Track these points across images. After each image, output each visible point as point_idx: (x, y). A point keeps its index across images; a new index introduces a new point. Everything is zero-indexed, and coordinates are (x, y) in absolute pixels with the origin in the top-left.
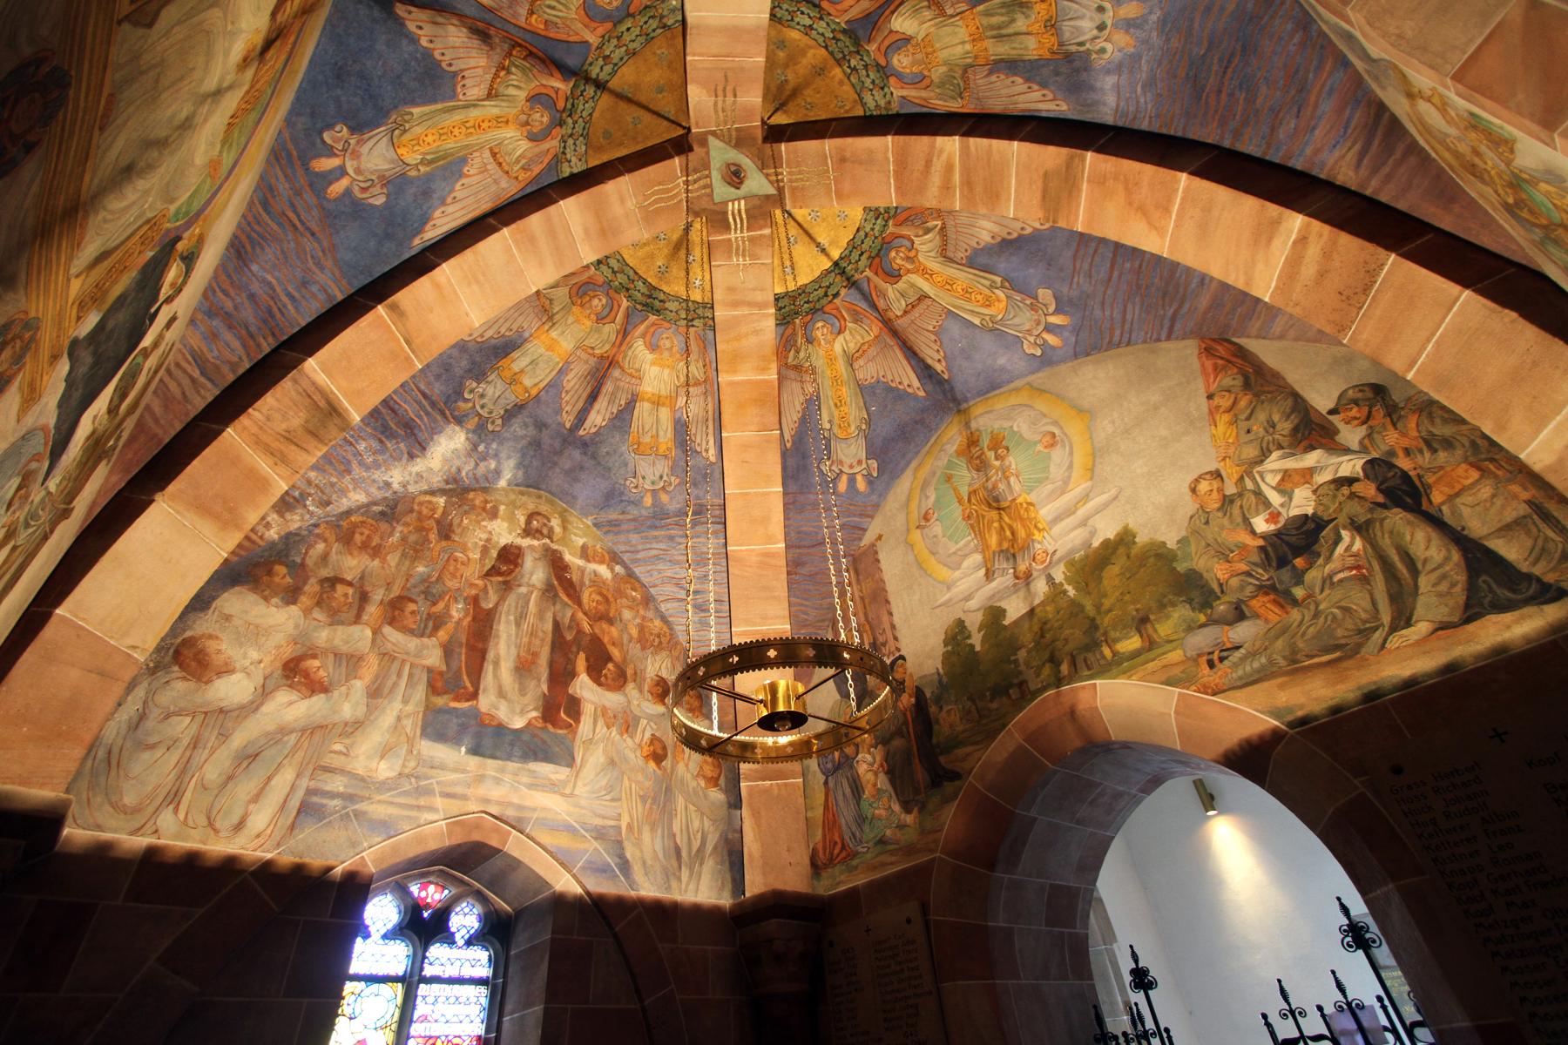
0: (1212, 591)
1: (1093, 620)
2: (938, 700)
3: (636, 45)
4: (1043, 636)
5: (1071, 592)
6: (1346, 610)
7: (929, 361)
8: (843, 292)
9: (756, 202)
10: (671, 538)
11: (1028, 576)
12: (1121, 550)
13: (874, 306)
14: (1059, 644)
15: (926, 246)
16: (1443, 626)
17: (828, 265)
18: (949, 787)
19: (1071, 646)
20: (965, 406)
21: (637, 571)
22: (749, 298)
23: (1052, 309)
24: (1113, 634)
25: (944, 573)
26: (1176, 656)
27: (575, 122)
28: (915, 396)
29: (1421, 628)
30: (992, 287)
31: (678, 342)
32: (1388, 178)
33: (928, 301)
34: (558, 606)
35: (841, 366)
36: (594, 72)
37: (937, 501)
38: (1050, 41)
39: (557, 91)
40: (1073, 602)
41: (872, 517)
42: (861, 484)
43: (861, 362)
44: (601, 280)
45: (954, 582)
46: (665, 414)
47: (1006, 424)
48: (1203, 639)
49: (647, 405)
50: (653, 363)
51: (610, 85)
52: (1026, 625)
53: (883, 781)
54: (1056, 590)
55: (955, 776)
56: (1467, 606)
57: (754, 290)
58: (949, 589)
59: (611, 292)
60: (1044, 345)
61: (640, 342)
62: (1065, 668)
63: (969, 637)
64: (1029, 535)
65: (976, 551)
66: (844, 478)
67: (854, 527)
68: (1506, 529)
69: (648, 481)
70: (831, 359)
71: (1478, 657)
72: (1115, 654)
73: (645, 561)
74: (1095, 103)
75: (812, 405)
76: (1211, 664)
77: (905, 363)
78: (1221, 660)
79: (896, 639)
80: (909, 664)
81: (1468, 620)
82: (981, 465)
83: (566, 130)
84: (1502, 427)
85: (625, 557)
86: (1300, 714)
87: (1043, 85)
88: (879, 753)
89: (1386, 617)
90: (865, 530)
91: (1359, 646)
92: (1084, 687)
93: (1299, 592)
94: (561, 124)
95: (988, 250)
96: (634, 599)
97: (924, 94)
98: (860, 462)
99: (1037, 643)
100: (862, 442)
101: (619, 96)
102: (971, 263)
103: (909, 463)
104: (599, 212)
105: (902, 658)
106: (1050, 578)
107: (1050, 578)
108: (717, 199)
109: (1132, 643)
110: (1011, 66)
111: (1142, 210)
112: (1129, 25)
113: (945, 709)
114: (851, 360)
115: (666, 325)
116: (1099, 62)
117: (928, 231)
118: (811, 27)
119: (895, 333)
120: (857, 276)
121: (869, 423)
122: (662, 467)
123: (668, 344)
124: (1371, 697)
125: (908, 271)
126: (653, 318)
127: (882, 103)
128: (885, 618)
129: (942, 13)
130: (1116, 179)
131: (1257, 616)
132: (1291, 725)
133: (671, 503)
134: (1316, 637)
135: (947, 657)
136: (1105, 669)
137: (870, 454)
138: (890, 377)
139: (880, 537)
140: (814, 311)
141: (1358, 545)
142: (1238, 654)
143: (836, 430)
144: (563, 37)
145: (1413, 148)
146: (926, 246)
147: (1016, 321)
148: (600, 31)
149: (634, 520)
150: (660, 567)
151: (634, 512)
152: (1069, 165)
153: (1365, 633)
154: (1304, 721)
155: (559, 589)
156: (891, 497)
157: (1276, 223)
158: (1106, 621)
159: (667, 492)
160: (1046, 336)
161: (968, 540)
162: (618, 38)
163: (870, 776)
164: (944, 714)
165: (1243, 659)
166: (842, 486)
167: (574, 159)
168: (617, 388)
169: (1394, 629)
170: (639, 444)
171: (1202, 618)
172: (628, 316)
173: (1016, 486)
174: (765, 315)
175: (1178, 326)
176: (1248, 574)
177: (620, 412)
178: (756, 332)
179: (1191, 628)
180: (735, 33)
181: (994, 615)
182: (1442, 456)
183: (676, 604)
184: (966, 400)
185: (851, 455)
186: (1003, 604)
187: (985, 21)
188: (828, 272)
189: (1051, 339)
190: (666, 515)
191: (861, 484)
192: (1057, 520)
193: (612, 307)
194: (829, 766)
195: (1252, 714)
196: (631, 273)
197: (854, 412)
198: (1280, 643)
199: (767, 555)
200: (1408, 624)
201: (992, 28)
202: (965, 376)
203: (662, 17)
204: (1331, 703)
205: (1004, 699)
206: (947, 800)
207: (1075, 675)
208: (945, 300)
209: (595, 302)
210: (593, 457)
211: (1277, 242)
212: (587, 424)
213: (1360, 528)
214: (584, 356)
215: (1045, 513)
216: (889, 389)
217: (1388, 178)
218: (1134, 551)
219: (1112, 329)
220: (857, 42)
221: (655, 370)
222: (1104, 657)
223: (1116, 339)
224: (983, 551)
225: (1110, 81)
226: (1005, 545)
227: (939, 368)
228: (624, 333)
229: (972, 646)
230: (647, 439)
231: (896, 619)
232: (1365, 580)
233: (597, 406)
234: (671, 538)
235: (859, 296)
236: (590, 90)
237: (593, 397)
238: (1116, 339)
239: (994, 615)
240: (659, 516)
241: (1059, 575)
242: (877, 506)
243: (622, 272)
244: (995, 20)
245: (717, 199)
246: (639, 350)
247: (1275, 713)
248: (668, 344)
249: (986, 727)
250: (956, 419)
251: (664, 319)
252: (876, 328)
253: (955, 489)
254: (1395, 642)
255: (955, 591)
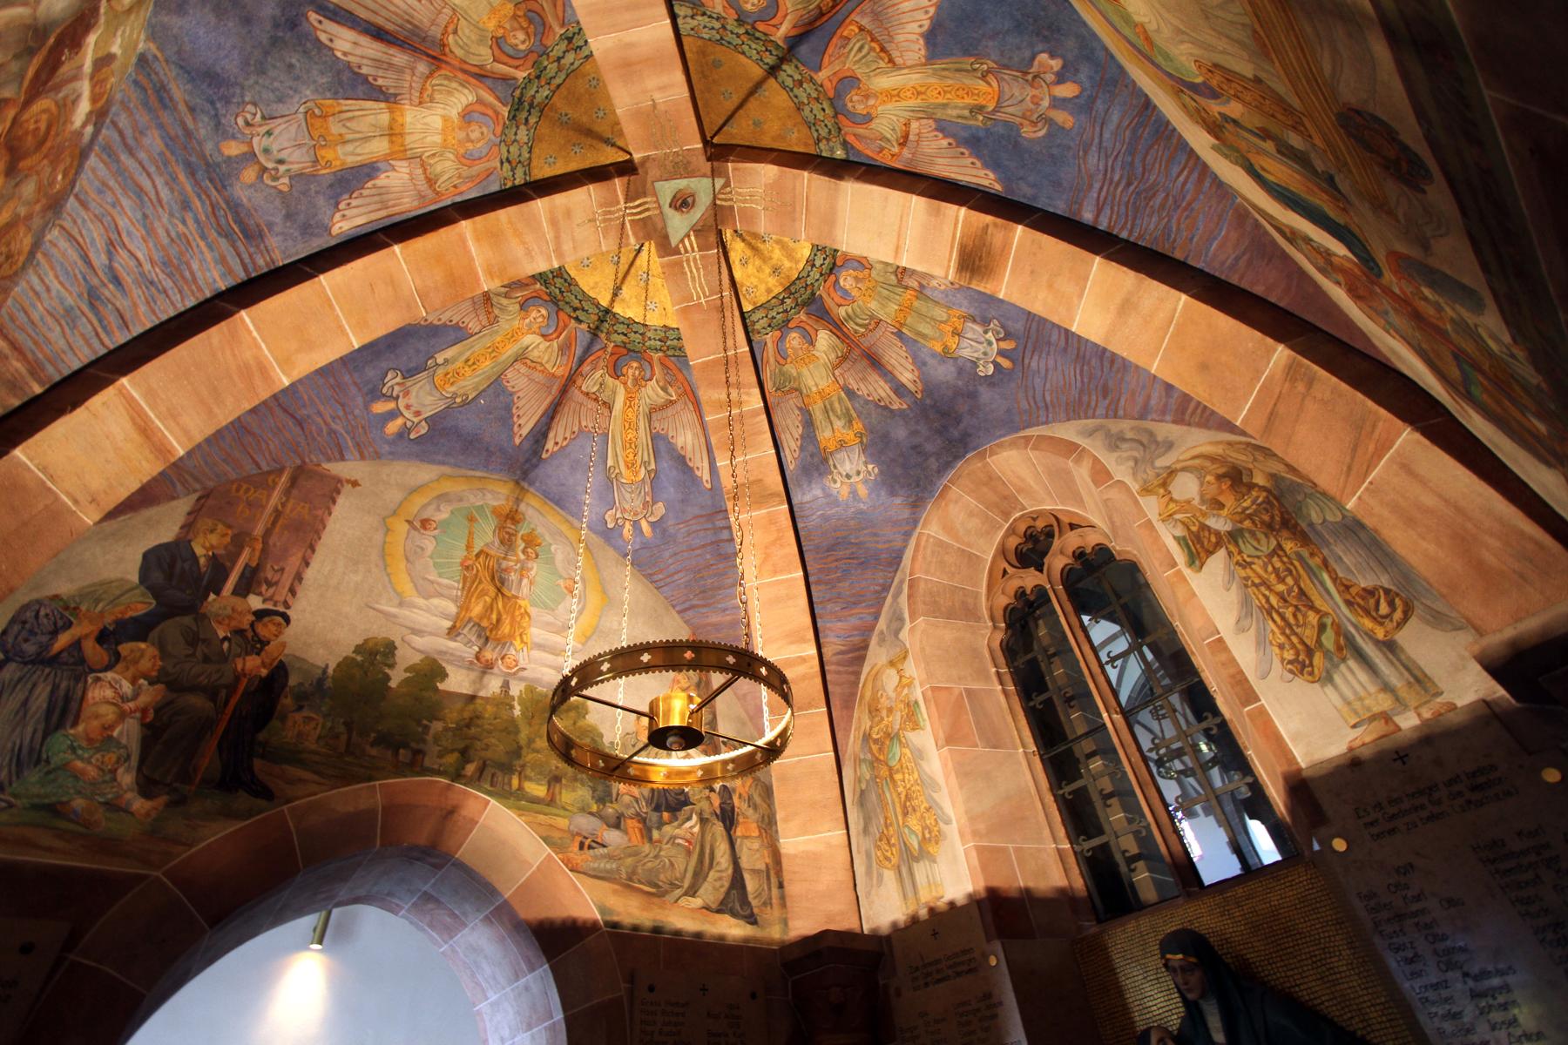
0: (610, 795)
1: (520, 748)
2: (302, 698)
3: (807, 111)
4: (468, 726)
5: (517, 712)
6: (672, 864)
7: (551, 435)
8: (584, 326)
9: (659, 226)
10: (186, 205)
11: (488, 667)
12: (572, 714)
13: (581, 362)
14: (478, 745)
15: (653, 392)
16: (707, 908)
17: (604, 303)
18: (243, 800)
19: (488, 754)
20: (526, 485)
21: (93, 161)
22: (563, 236)
23: (652, 519)
24: (528, 772)
25: (407, 587)
26: (562, 823)
27: (738, 36)
28: (512, 436)
29: (697, 902)
30: (645, 464)
31: (480, 147)
32: (838, 673)
33: (606, 412)
34: (14, 67)
35: (510, 351)
36: (788, 68)
37: (446, 523)
38: (832, 447)
39: (776, 27)
40: (513, 720)
41: (363, 458)
42: (393, 427)
43: (523, 369)
44: (548, 42)
45: (412, 606)
46: (379, 147)
47: (547, 537)
48: (586, 823)
49: (385, 118)
50: (445, 119)
51: (772, 81)
52: (459, 705)
53: (129, 732)
54: (504, 700)
55: (267, 794)
56: (721, 903)
57: (573, 240)
58: (401, 605)
59: (533, 57)
60: (619, 528)
61: (471, 98)
62: (470, 769)
63: (392, 666)
64: (511, 636)
65: (455, 600)
66: (391, 405)
67: (338, 445)
68: (755, 872)
69: (266, 142)
70: (513, 336)
71: (713, 937)
72: (520, 788)
73: (120, 172)
74: (800, 486)
75: (458, 334)
76: (581, 846)
77: (540, 412)
78: (590, 847)
79: (293, 592)
80: (290, 633)
81: (718, 911)
82: (507, 542)
83: (731, 24)
84: (786, 820)
85: (107, 132)
86: (616, 918)
87: (802, 448)
88: (150, 695)
89: (686, 884)
90: (343, 458)
91: (666, 892)
92: (477, 797)
93: (656, 834)
94: (740, 21)
95: (671, 448)
96: (52, 183)
97: (772, 360)
98: (418, 413)
99: (459, 728)
100: (441, 406)
101: (758, 85)
102: (656, 438)
103: (444, 463)
104: (653, 62)
105: (287, 620)
106: (506, 685)
107: (506, 685)
108: (658, 185)
109: (538, 789)
110: (809, 423)
111: (767, 557)
112: (854, 493)
113: (306, 713)
114: (521, 357)
115: (499, 130)
116: (827, 481)
117: (664, 389)
118: (813, 266)
119: (564, 391)
120: (603, 336)
121: (465, 403)
122: (298, 160)
123: (475, 135)
124: (657, 930)
125: (625, 384)
126: (505, 111)
127: (757, 326)
128: (293, 562)
129: (835, 367)
130: (778, 530)
131: (626, 832)
132: (607, 924)
133: (244, 187)
134: (650, 870)
135: (346, 663)
136: (505, 795)
137: (431, 420)
138: (520, 404)
139: (355, 484)
140: (554, 301)
141: (696, 829)
142: (602, 851)
143: (440, 371)
144: (830, 50)
145: (858, 674)
146: (653, 392)
147: (628, 496)
148: (828, 85)
149: (188, 134)
150: (125, 202)
151: (203, 129)
152: (773, 495)
153: (674, 886)
154: (615, 925)
155: (44, 52)
156: (399, 466)
157: (804, 640)
158: (529, 757)
159: (260, 177)
160: (628, 526)
161: (452, 583)
162: (817, 99)
163: (109, 713)
164: (298, 716)
165: (603, 856)
166: (380, 407)
167: (694, 23)
168: (400, 70)
169: (686, 894)
170: (324, 117)
171: (594, 808)
172: (505, 79)
173: (525, 590)
174: (549, 259)
175: (690, 613)
176: (637, 801)
177: (365, 79)
178: (529, 253)
179: (584, 810)
180: (830, 220)
181: (432, 671)
182: (751, 811)
183: (73, 255)
184: (531, 484)
185: (420, 400)
186: (449, 669)
187: (835, 399)
188: (597, 305)
189: (627, 530)
190: (221, 186)
191: (393, 427)
192: (540, 647)
193: (515, 58)
194: (30, 648)
195: (585, 900)
196: (558, 81)
197: (470, 384)
198: (629, 860)
199: (264, 370)
200: (693, 896)
201: (831, 405)
202: (554, 473)
203: (828, 140)
204: (637, 922)
205: (389, 754)
206: (230, 814)
207: (476, 780)
208: (615, 427)
209: (521, 36)
210: (274, 41)
211: (793, 647)
212: (329, 26)
213: (703, 821)
214: (443, 19)
215: (536, 633)
216: (508, 408)
217: (838, 673)
218: (580, 723)
219: (661, 571)
220: (804, 304)
221: (437, 122)
222: (510, 784)
223: (656, 578)
224: (461, 608)
225: (818, 492)
226: (485, 623)
227: (550, 445)
228: (481, 76)
229: (388, 678)
230: (335, 128)
231: (309, 574)
232: (689, 853)
233: (365, 41)
234: (186, 205)
235: (585, 343)
236: (770, 60)
237: (378, 34)
238: (656, 578)
239: (432, 671)
240: (216, 175)
241: (516, 689)
242: (378, 456)
243: (560, 70)
244: (837, 405)
245: (658, 185)
246: (463, 97)
247: (602, 910)
248: (475, 135)
249: (346, 765)
250: (511, 485)
251: (505, 126)
252: (561, 371)
253: (471, 534)
254: (683, 901)
255: (405, 612)
